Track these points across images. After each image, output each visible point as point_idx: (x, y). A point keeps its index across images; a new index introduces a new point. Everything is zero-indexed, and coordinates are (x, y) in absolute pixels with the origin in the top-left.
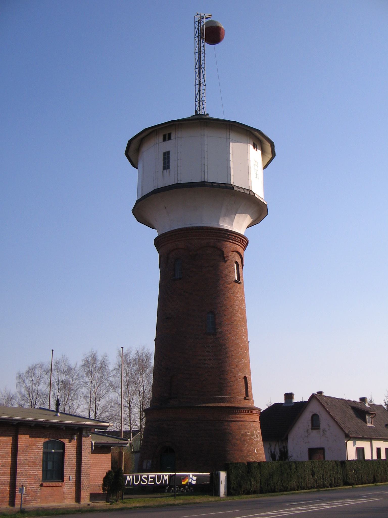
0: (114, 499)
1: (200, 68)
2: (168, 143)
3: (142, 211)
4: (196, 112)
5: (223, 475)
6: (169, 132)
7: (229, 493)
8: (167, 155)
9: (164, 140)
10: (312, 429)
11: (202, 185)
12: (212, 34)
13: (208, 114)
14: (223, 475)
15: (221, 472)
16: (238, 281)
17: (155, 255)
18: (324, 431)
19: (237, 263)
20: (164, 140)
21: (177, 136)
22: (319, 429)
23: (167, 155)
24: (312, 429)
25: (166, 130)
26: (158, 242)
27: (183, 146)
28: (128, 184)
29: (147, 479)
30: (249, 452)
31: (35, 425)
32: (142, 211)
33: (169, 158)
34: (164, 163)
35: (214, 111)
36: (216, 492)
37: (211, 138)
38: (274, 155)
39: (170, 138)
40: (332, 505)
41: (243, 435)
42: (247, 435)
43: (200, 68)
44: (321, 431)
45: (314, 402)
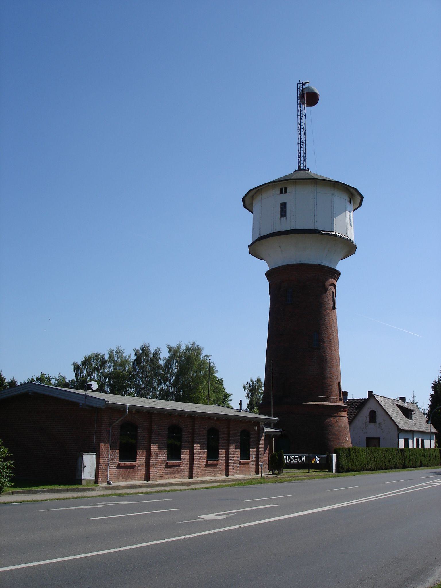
0: (5, 477)
1: (301, 129)
2: (284, 195)
3: (255, 249)
4: (300, 167)
5: (335, 456)
6: (285, 186)
7: (338, 471)
8: (283, 206)
9: (281, 192)
10: (370, 422)
11: (314, 231)
12: (309, 98)
13: (308, 169)
14: (335, 456)
15: (118, 451)
16: (334, 308)
17: (266, 284)
18: (380, 424)
19: (333, 292)
20: (281, 192)
21: (292, 190)
22: (376, 422)
23: (283, 206)
24: (370, 422)
25: (282, 185)
26: (269, 275)
27: (295, 198)
28: (243, 227)
29: (294, 458)
30: (343, 440)
31: (217, 419)
32: (255, 249)
33: (285, 208)
34: (281, 212)
35: (318, 168)
36: (330, 470)
37: (323, 195)
38: (360, 205)
39: (286, 192)
40: (165, 485)
41: (339, 427)
42: (341, 427)
43: (301, 129)
44: (378, 423)
45: (372, 400)
